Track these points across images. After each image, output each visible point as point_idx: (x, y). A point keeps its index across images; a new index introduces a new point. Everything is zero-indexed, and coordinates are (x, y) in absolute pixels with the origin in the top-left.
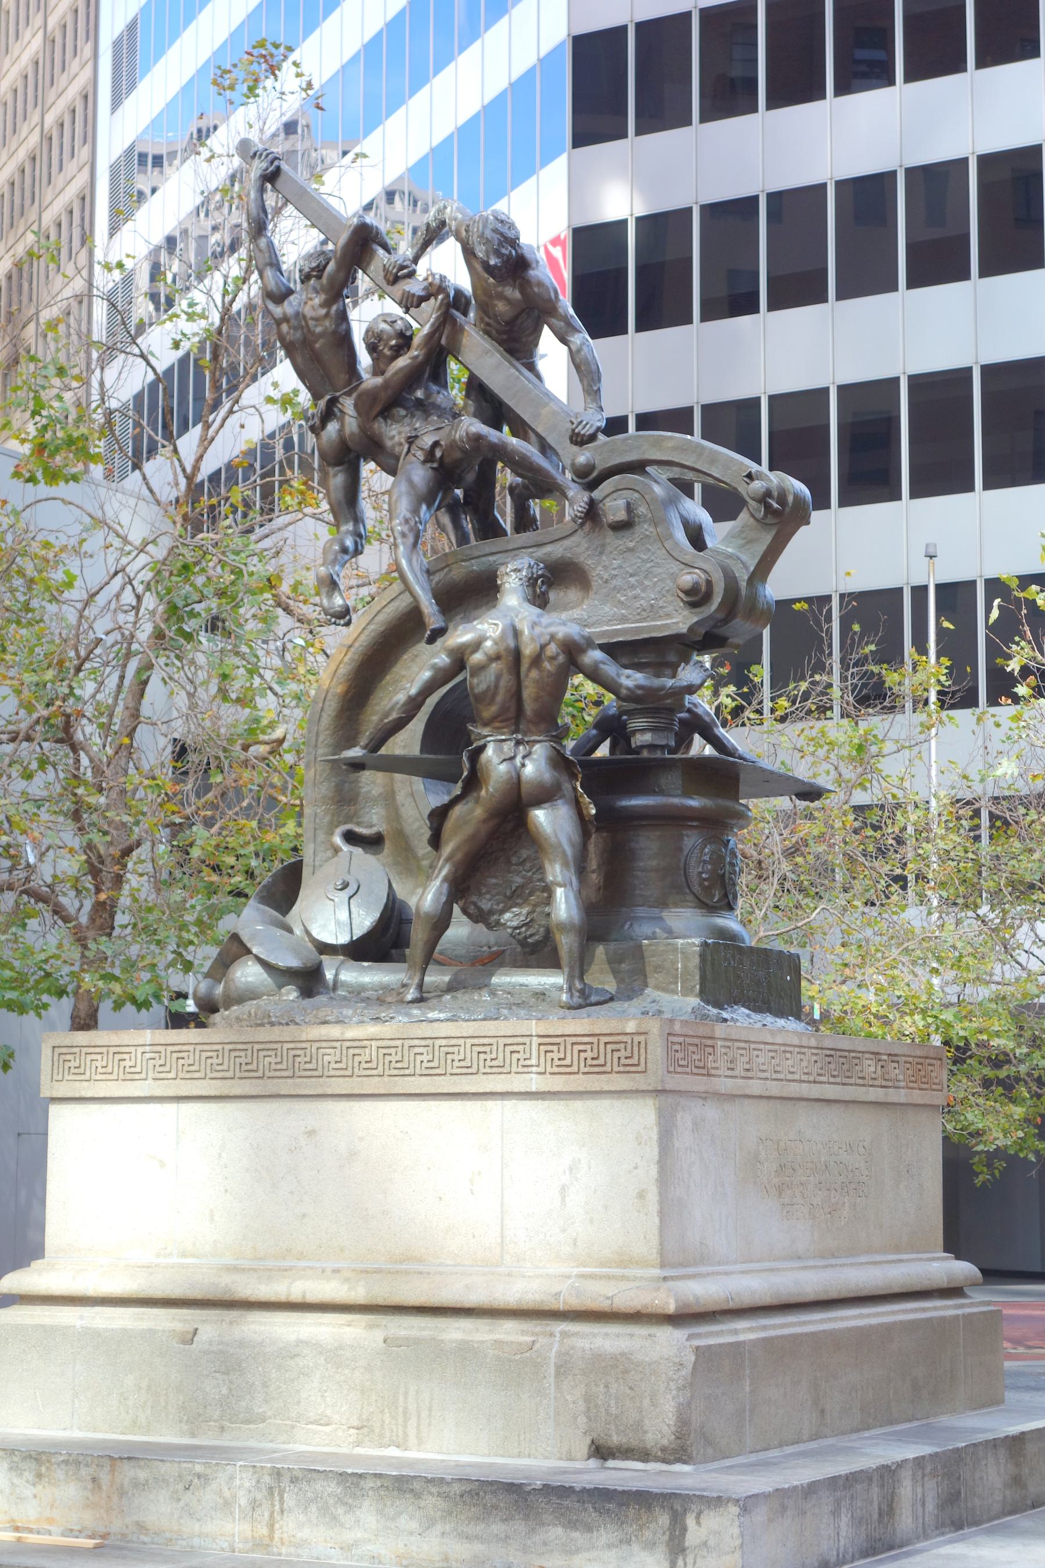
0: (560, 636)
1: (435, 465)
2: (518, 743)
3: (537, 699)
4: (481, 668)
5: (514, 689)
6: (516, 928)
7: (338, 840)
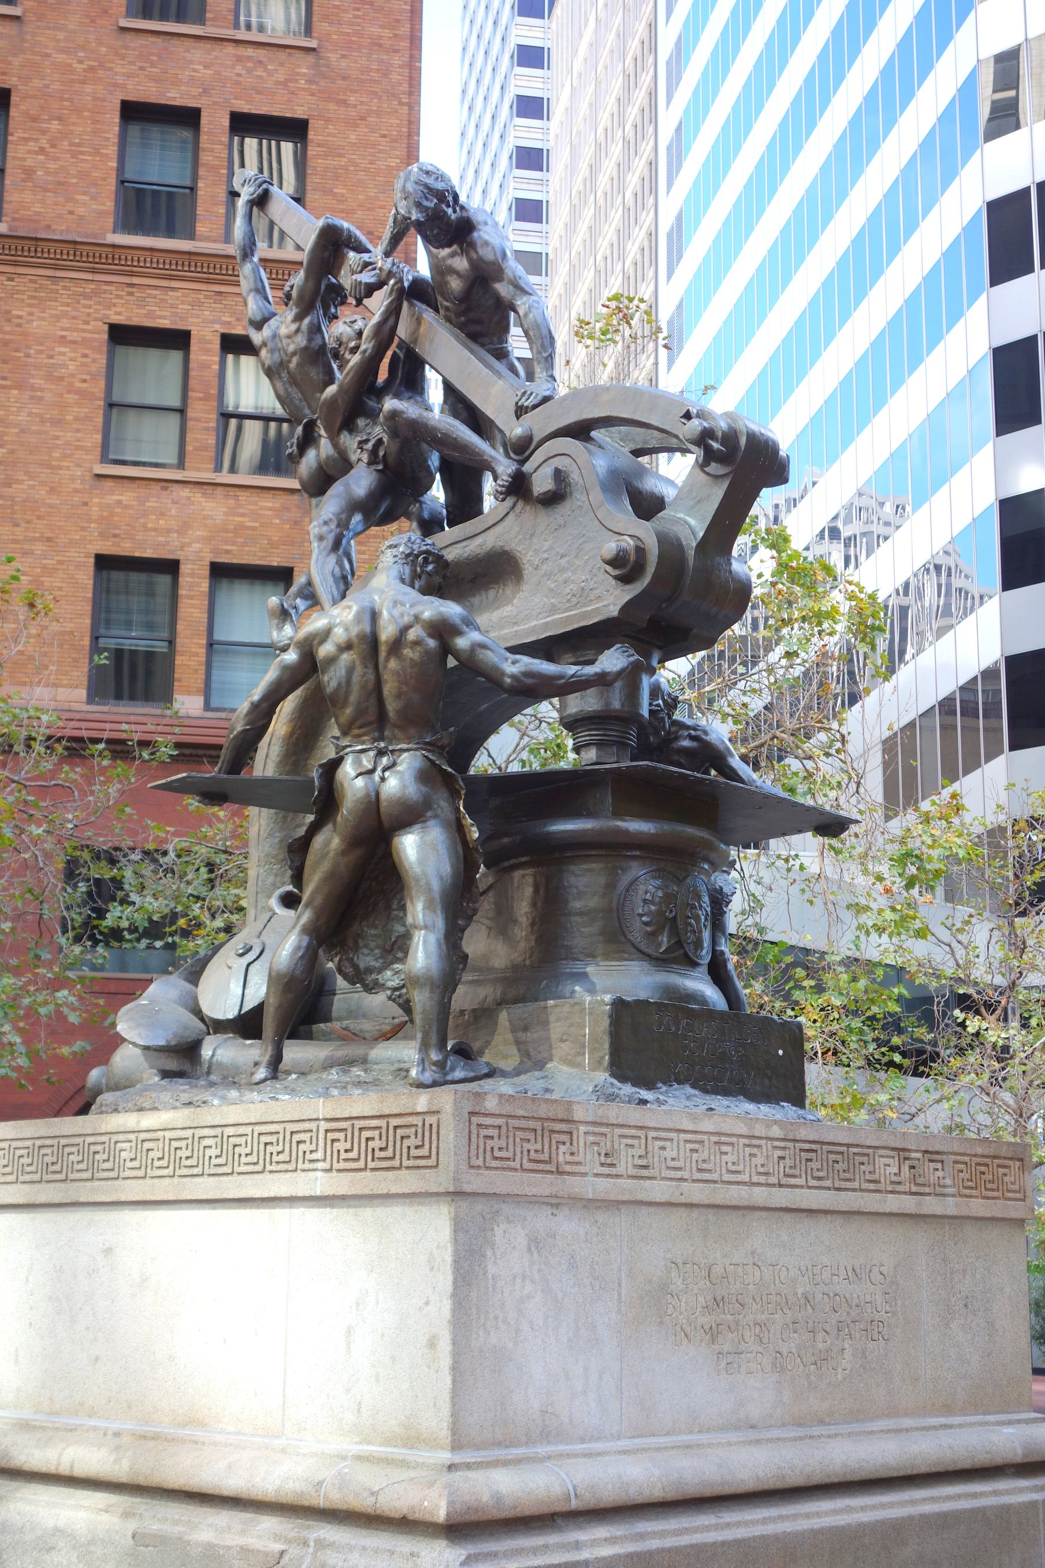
0: (427, 615)
1: (380, 467)
2: (381, 753)
3: (399, 696)
4: (331, 660)
5: (371, 685)
6: (395, 989)
7: (274, 903)
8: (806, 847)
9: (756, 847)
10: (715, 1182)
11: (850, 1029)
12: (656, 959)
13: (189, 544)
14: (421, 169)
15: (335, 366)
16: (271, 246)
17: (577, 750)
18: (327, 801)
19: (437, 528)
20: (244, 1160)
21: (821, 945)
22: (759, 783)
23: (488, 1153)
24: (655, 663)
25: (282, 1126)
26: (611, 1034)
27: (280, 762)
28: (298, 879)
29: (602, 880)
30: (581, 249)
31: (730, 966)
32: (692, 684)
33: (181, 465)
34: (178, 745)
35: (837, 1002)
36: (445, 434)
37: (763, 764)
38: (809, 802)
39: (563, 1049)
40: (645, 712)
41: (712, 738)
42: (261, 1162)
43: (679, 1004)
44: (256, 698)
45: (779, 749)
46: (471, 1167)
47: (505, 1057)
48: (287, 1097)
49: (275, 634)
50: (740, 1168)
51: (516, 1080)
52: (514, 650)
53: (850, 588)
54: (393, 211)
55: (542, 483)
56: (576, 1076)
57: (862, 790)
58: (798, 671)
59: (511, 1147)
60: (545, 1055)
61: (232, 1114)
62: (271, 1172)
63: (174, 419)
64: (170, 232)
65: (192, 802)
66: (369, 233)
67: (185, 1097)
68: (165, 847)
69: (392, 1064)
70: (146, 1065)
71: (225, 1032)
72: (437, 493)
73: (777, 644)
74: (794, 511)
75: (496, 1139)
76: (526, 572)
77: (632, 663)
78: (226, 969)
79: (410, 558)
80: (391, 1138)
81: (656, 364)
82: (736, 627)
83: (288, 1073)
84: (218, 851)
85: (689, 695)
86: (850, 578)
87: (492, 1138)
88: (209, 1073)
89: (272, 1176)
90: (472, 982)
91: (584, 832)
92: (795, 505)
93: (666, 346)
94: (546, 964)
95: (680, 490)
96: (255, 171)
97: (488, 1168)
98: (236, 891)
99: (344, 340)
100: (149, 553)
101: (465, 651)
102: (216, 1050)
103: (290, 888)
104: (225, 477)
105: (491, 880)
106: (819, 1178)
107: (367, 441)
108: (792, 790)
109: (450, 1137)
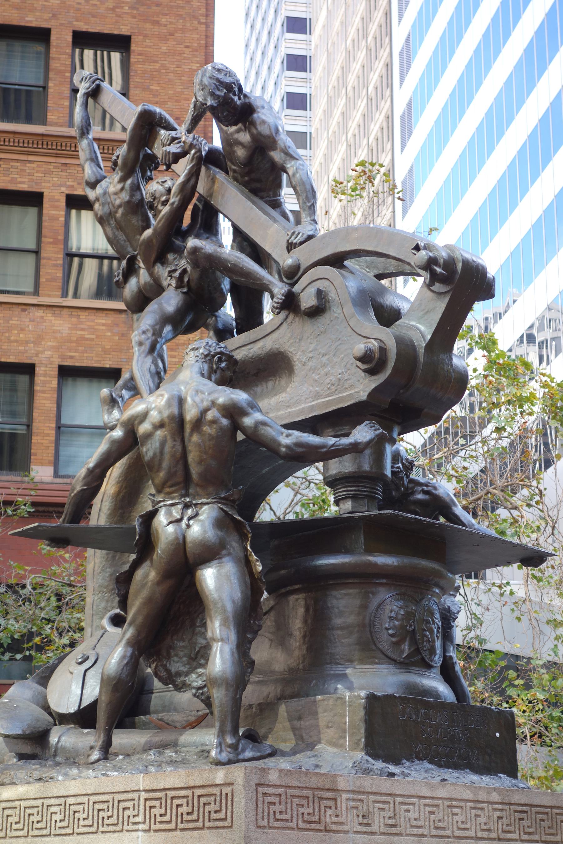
0: (221, 400)
1: (185, 290)
2: (187, 506)
3: (200, 462)
4: (149, 436)
5: (179, 454)
6: (199, 688)
7: (105, 622)
8: (514, 576)
9: (476, 577)
10: (448, 837)
11: (551, 718)
12: (400, 663)
13: (43, 352)
14: (214, 68)
15: (150, 215)
16: (104, 128)
17: (337, 503)
18: (146, 544)
19: (228, 336)
20: (82, 823)
21: (526, 652)
22: (477, 526)
23: (272, 816)
24: (395, 435)
25: (112, 796)
26: (366, 722)
27: (110, 514)
28: (124, 604)
29: (358, 602)
30: (336, 129)
31: (458, 668)
32: (424, 453)
33: (36, 292)
34: (34, 504)
35: (541, 697)
36: (235, 265)
37: (480, 513)
38: (515, 540)
39: (328, 734)
40: (388, 473)
41: (440, 492)
42: (95, 824)
43: (419, 698)
44: (91, 465)
45: (492, 502)
46: (258, 827)
47: (284, 741)
48: (115, 773)
49: (106, 417)
50: (468, 826)
51: (292, 758)
52: (287, 426)
53: (544, 379)
54: (194, 99)
55: (307, 300)
56: (339, 756)
57: (556, 532)
58: (505, 442)
59: (289, 811)
60: (315, 738)
61: (73, 787)
62: (103, 832)
63: (31, 258)
64: (29, 120)
65: (44, 547)
66: (177, 119)
67: (36, 774)
68: (24, 581)
69: (197, 747)
70: (6, 750)
71: (68, 723)
72: (229, 310)
73: (489, 422)
74: (500, 322)
75: (277, 805)
76: (296, 367)
77: (377, 435)
78: (69, 674)
79: (208, 357)
80: (196, 805)
81: (394, 212)
82: (456, 408)
83: (116, 754)
84: (64, 585)
85: (422, 461)
86: (544, 372)
87: (274, 804)
88: (55, 755)
89: (103, 835)
90: (258, 682)
91: (343, 565)
92: (500, 318)
93: (399, 198)
94: (314, 668)
95: (413, 304)
96: (92, 70)
97: (271, 828)
98: (79, 615)
99: (157, 195)
100: (12, 359)
101: (250, 427)
102: (62, 737)
103: (118, 611)
104: (70, 301)
105: (272, 603)
106: (530, 834)
107: (175, 270)
108: (503, 533)
109: (241, 803)
